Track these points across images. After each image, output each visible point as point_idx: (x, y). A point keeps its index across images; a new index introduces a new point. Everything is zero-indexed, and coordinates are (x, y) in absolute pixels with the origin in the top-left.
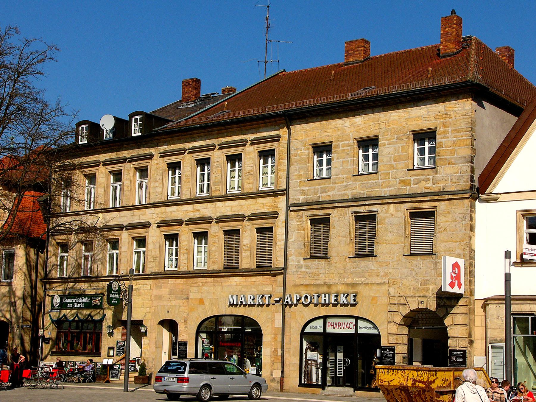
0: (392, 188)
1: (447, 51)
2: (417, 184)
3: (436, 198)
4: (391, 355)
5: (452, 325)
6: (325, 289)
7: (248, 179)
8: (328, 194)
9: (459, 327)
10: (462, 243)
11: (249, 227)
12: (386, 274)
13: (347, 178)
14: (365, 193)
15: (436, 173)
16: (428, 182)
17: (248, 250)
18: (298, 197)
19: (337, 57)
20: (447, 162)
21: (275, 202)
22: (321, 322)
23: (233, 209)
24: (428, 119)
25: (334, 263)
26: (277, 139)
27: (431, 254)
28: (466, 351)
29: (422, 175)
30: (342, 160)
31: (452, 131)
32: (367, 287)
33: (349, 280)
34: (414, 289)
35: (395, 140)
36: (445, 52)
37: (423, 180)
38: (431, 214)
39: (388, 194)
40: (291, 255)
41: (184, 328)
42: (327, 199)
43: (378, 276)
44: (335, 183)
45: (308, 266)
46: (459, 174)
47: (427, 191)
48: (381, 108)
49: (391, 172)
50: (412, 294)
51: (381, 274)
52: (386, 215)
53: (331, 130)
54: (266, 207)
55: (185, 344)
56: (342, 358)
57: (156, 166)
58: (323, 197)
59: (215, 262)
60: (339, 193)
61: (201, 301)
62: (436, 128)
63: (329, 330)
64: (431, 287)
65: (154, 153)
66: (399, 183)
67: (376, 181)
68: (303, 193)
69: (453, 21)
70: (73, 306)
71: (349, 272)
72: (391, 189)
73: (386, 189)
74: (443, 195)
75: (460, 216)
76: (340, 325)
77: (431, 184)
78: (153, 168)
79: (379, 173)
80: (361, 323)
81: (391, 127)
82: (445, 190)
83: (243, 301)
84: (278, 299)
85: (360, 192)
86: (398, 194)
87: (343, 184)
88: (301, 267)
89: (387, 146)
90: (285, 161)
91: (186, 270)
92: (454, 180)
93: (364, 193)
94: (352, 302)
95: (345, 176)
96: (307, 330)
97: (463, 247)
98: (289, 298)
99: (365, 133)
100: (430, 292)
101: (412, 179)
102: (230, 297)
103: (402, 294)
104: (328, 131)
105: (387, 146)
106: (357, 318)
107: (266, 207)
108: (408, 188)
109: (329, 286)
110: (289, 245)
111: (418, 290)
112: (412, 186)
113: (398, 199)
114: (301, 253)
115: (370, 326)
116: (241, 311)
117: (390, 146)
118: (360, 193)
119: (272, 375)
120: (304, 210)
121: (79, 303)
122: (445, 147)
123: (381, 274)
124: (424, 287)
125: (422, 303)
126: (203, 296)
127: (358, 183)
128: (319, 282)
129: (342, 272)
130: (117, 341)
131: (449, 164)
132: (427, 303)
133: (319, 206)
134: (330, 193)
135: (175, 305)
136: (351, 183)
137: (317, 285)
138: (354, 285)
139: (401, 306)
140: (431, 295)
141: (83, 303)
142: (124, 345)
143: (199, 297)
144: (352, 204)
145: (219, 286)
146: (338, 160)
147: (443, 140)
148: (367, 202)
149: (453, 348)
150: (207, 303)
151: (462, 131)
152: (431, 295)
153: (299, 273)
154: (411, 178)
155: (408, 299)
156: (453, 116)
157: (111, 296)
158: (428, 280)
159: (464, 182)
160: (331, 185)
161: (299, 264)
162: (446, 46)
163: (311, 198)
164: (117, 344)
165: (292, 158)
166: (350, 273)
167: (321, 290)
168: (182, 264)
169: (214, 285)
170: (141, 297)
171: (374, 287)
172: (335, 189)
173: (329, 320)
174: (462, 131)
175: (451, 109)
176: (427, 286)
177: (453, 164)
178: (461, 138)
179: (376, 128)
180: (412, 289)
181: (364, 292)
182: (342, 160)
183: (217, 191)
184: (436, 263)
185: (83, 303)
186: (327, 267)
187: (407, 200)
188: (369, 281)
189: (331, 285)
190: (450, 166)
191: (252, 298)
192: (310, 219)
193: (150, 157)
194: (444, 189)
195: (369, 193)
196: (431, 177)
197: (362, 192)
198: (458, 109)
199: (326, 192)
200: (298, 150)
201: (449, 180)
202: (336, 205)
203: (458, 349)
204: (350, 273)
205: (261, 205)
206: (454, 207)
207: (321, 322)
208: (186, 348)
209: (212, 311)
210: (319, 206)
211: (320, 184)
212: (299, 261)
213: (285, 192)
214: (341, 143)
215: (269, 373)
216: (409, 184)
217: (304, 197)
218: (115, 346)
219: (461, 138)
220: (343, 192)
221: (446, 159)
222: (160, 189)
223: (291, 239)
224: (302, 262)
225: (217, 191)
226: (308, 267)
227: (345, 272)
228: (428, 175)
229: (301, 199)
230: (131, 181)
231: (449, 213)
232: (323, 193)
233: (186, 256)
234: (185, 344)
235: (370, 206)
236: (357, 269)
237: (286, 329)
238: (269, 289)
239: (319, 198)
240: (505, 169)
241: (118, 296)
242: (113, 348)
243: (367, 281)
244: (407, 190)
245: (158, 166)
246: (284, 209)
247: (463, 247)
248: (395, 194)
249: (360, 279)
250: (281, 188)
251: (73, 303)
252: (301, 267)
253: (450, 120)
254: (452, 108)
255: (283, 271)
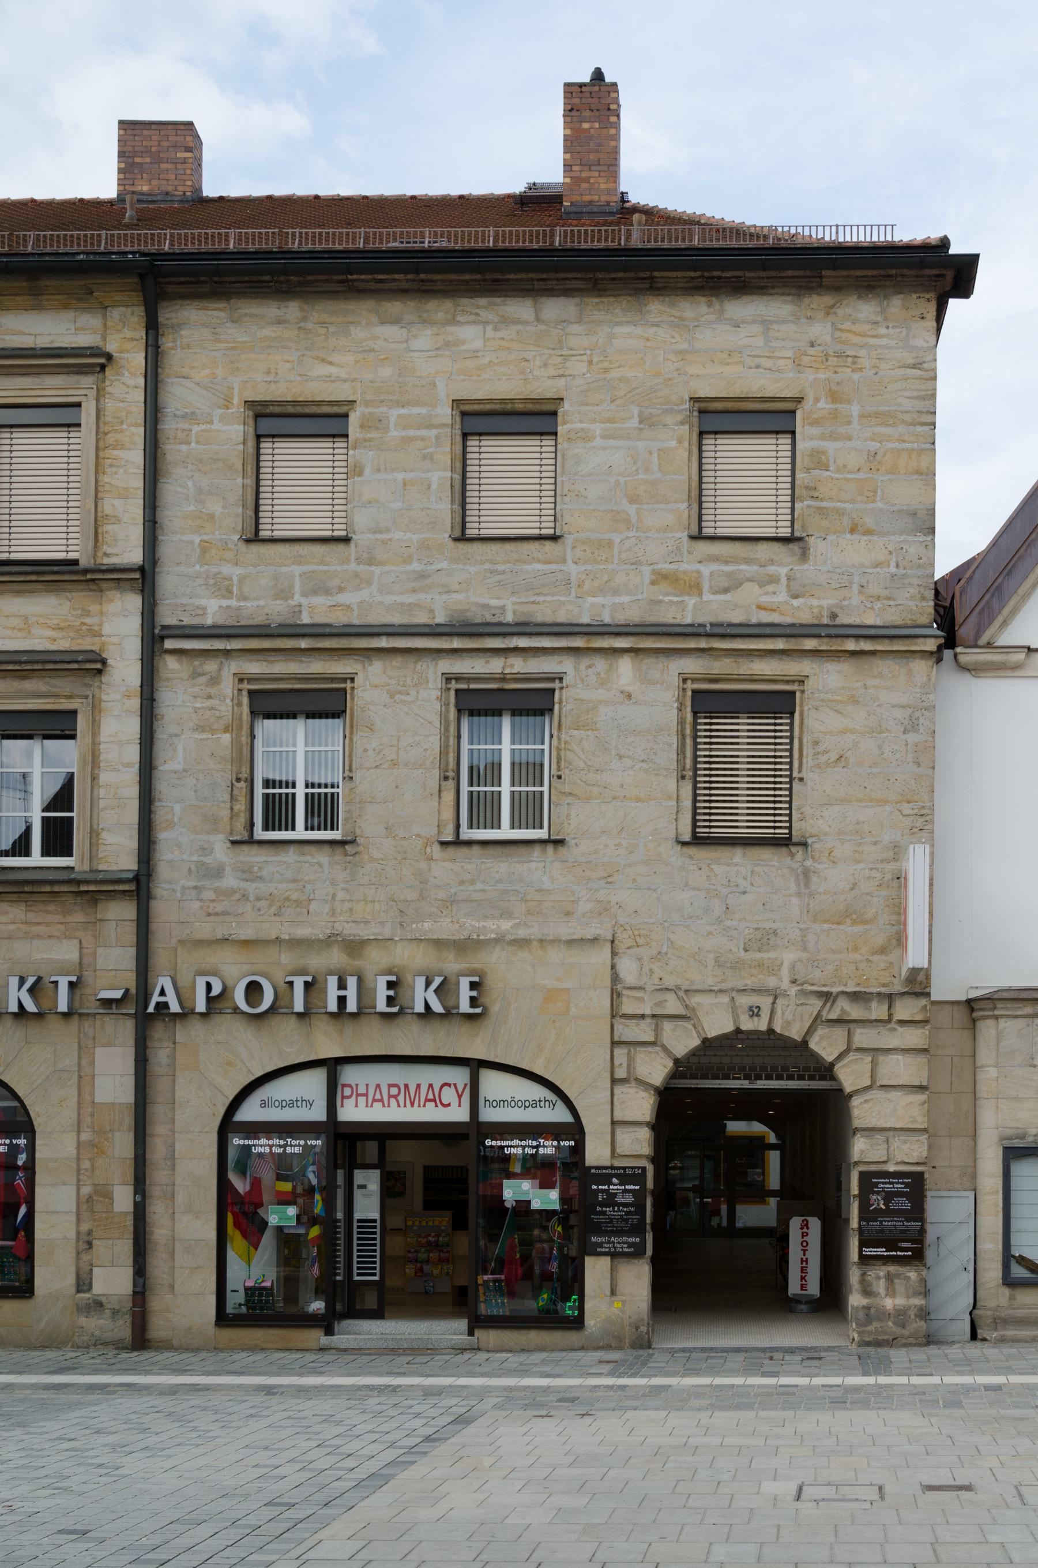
0: (625, 599)
1: (587, 198)
2: (726, 591)
3: (810, 644)
4: (629, 1199)
5: (869, 1088)
6: (336, 958)
8: (344, 598)
9: (893, 1095)
10: (907, 809)
12: (604, 909)
13: (423, 546)
14: (510, 608)
15: (804, 555)
16: (770, 588)
18: (197, 602)
19: (91, 175)
20: (847, 522)
21: (87, 613)
22: (310, 1086)
24: (769, 363)
25: (372, 859)
26: (97, 362)
27: (784, 842)
28: (922, 1174)
29: (748, 561)
30: (400, 476)
31: (862, 416)
32: (524, 954)
33: (445, 928)
34: (719, 963)
35: (634, 423)
36: (576, 198)
37: (750, 580)
38: (778, 704)
39: (607, 620)
40: (171, 825)
42: (338, 618)
43: (567, 914)
44: (371, 561)
45: (249, 871)
46: (893, 569)
47: (766, 617)
48: (577, 300)
49: (616, 538)
50: (710, 982)
51: (584, 907)
52: (601, 694)
53: (350, 358)
54: (37, 631)
56: (376, 1215)
58: (315, 610)
60: (389, 599)
62: (799, 400)
63: (351, 1112)
64: (788, 957)
66: (653, 583)
67: (553, 567)
68: (223, 588)
69: (592, 105)
71: (442, 894)
72: (617, 600)
73: (599, 600)
74: (834, 638)
75: (898, 713)
76: (409, 1095)
77: (782, 597)
79: (569, 540)
80: (493, 1084)
81: (615, 374)
82: (839, 621)
83: (171, 999)
85: (483, 601)
86: (651, 619)
87: (409, 568)
88: (218, 872)
89: (599, 442)
90: (136, 457)
92: (874, 589)
93: (503, 608)
94: (465, 1007)
95: (415, 537)
96: (250, 1112)
97: (908, 822)
99: (500, 384)
100: (785, 973)
101: (706, 570)
103: (670, 981)
104: (335, 358)
105: (599, 442)
106: (476, 1066)
107: (37, 631)
108: (691, 601)
109: (355, 947)
110: (163, 787)
111: (736, 966)
112: (707, 596)
113: (650, 638)
114: (216, 820)
115: (538, 1092)
117: (612, 442)
118: (486, 606)
119: (83, 1284)
120: (227, 653)
122: (838, 471)
123: (584, 907)
124: (758, 956)
125: (754, 1012)
127: (473, 569)
128: (302, 932)
129: (411, 895)
131: (852, 531)
132: (773, 1012)
133: (304, 644)
134: (347, 598)
136: (444, 565)
137: (296, 943)
138: (463, 946)
139: (667, 1026)
140: (785, 984)
144: (456, 643)
146: (383, 476)
147: (830, 446)
148: (523, 642)
149: (873, 1168)
151: (903, 422)
152: (785, 984)
153: (208, 895)
154: (702, 568)
155: (695, 1000)
156: (864, 362)
158: (775, 933)
159: (912, 598)
160: (353, 566)
161: (208, 860)
162: (587, 180)
163: (268, 608)
165: (172, 450)
166: (451, 902)
167: (316, 962)
171: (554, 955)
172: (369, 583)
173: (350, 1075)
174: (903, 422)
175: (857, 339)
176: (772, 955)
177: (868, 532)
178: (897, 445)
179: (551, 371)
180: (711, 962)
181: (505, 970)
182: (400, 476)
184: (807, 874)
186: (341, 876)
187: (692, 644)
188: (533, 930)
189: (363, 943)
190: (856, 537)
192: (251, 693)
194: (834, 616)
195: (526, 609)
196: (783, 571)
197: (494, 602)
198: (884, 341)
199: (327, 592)
201: (855, 588)
202: (383, 643)
203: (891, 1168)
204: (451, 902)
206: (876, 682)
207: (310, 1086)
210: (304, 644)
211: (299, 561)
212: (205, 850)
214: (394, 413)
216: (695, 587)
217: (225, 603)
219: (897, 445)
220: (407, 599)
221: (841, 513)
223: (172, 761)
224: (221, 851)
226: (248, 873)
227: (422, 897)
228: (772, 561)
229: (213, 610)
231: (854, 700)
232: (315, 592)
235: (135, 703)
236: (479, 886)
237: (158, 1111)
239: (298, 610)
243: (522, 933)
244: (687, 611)
246: (133, 647)
247: (908, 822)
248: (636, 620)
249: (491, 925)
250: (106, 561)
252: (218, 872)
253: (856, 376)
254: (863, 335)
255: (140, 885)
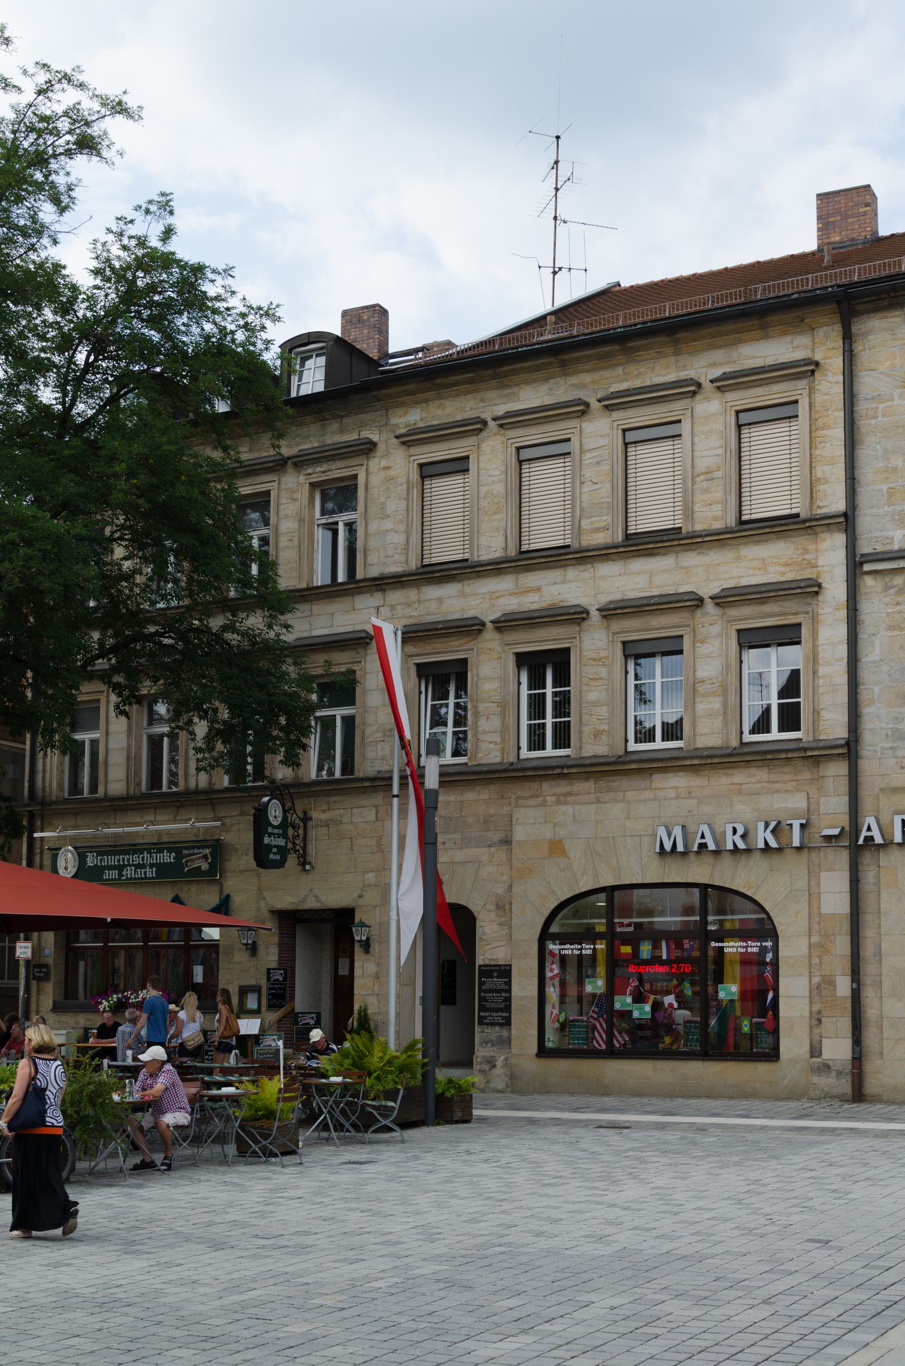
7: (707, 491)
11: (715, 629)
17: (714, 694)
18: (886, 534)
21: (806, 551)
23: (657, 580)
26: (808, 369)
41: (496, 927)
55: (505, 972)
57: (383, 474)
59: (597, 734)
61: (556, 848)
65: (375, 438)
70: (121, 875)
78: (376, 480)
84: (836, 832)
90: (838, 433)
91: (498, 760)
98: (874, 827)
102: (662, 832)
107: (771, 569)
110: (865, 674)
116: (699, 872)
119: (815, 1051)
121: (142, 866)
126: (562, 832)
130: (269, 970)
135: (463, 863)
141: (151, 866)
142: (285, 979)
143: (548, 835)
145: (615, 801)
150: (576, 852)
157: (266, 840)
164: (269, 979)
165: (865, 424)
168: (483, 746)
169: (598, 801)
170: (347, 843)
183: (597, 530)
185: (151, 866)
191: (740, 831)
193: (368, 448)
200: (878, 398)
205: (755, 563)
208: (509, 983)
209: (596, 876)
213: (847, 521)
215: (806, 1048)
218: (263, 982)
222: (400, 539)
225: (597, 530)
230: (301, 521)
233: (496, 722)
234: (505, 972)
237: (868, 919)
238: (798, 802)
240: (523, 369)
241: (281, 842)
242: (257, 989)
245: (391, 473)
246: (841, 572)
250: (819, 511)
251: (120, 868)
